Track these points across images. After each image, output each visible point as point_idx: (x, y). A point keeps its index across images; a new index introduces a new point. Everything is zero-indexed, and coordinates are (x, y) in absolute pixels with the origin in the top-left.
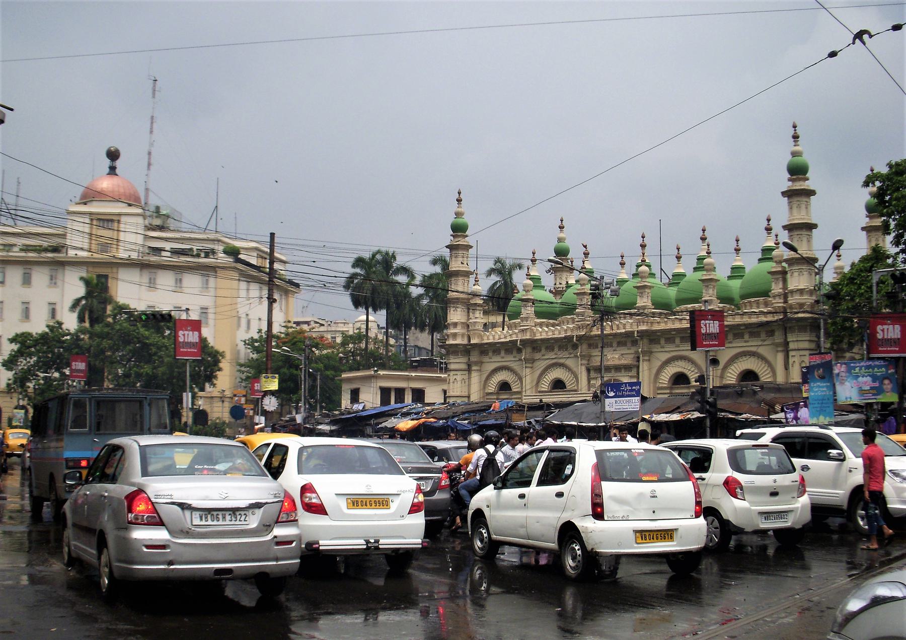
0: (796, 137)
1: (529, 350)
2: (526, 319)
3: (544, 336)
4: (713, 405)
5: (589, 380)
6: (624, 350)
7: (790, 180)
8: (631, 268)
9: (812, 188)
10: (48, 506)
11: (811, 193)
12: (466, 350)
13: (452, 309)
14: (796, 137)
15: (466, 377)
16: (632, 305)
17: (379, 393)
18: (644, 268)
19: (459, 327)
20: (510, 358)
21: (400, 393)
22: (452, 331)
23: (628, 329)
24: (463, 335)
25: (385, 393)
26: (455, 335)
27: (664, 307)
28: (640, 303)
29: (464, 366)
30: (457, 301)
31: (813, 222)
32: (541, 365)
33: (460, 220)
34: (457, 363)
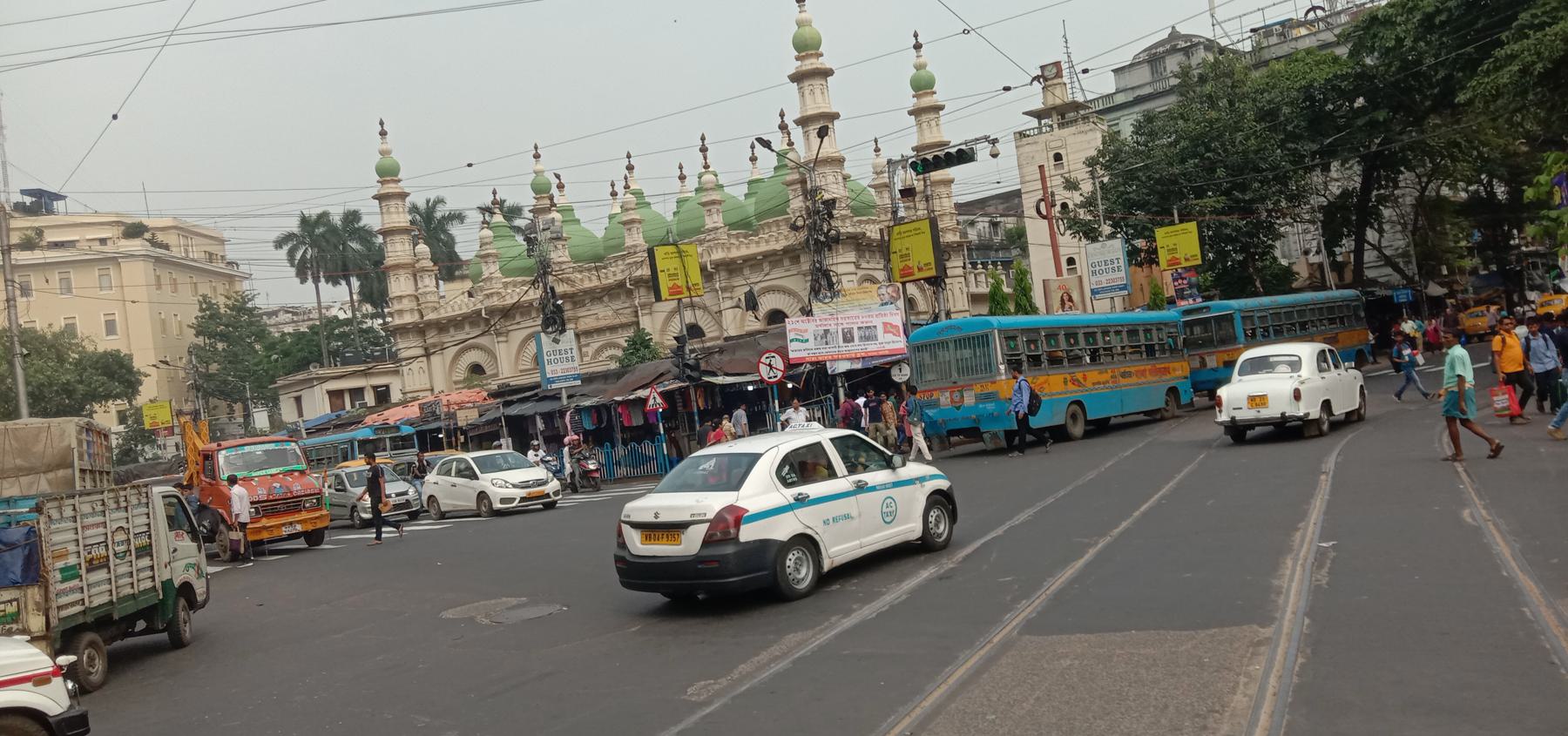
0: (383, 134)
1: (723, 274)
2: (489, 279)
3: (587, 285)
4: (696, 368)
5: (580, 349)
6: (617, 305)
7: (797, 59)
8: (692, 183)
9: (828, 66)
10: (798, 562)
11: (826, 73)
12: (420, 329)
13: (392, 279)
14: (383, 134)
15: (424, 365)
16: (619, 247)
17: (326, 397)
18: (708, 177)
19: (405, 301)
20: (776, 273)
21: (357, 393)
22: (396, 306)
23: (620, 277)
24: (412, 310)
25: (335, 395)
26: (400, 312)
27: (744, 226)
28: (629, 242)
29: (420, 351)
30: (397, 266)
31: (834, 110)
32: (518, 337)
33: (387, 161)
34: (408, 347)
